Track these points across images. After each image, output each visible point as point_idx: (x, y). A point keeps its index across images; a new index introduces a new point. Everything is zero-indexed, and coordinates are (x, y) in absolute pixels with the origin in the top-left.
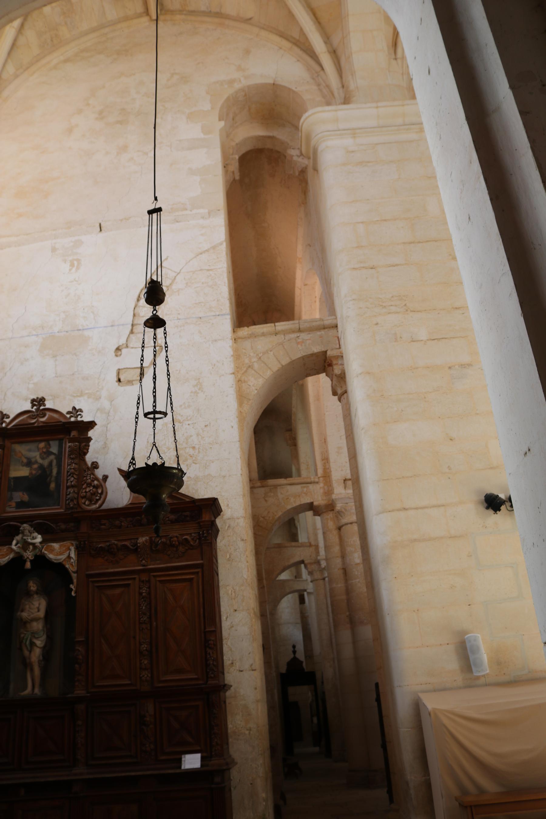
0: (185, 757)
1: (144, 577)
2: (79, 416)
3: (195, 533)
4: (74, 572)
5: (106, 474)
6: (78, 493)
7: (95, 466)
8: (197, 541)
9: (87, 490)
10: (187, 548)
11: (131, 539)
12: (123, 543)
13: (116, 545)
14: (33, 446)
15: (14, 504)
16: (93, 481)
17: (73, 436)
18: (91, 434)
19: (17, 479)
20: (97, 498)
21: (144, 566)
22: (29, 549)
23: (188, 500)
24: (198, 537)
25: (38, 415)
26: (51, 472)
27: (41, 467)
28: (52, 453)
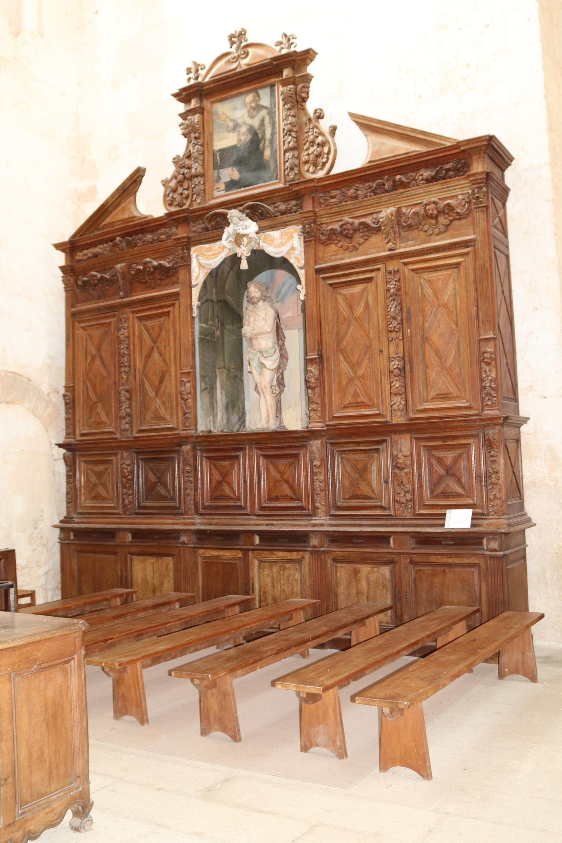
0: (450, 513)
1: (393, 266)
2: (293, 46)
3: (463, 194)
4: (301, 268)
5: (334, 124)
6: (298, 158)
9: (310, 152)
10: (451, 218)
11: (372, 214)
12: (361, 221)
13: (352, 224)
14: (237, 102)
15: (223, 186)
16: (317, 137)
17: (286, 76)
18: (311, 69)
20: (324, 160)
21: (390, 250)
22: (243, 243)
23: (448, 144)
24: (468, 200)
25: (239, 56)
26: (264, 134)
28: (263, 107)
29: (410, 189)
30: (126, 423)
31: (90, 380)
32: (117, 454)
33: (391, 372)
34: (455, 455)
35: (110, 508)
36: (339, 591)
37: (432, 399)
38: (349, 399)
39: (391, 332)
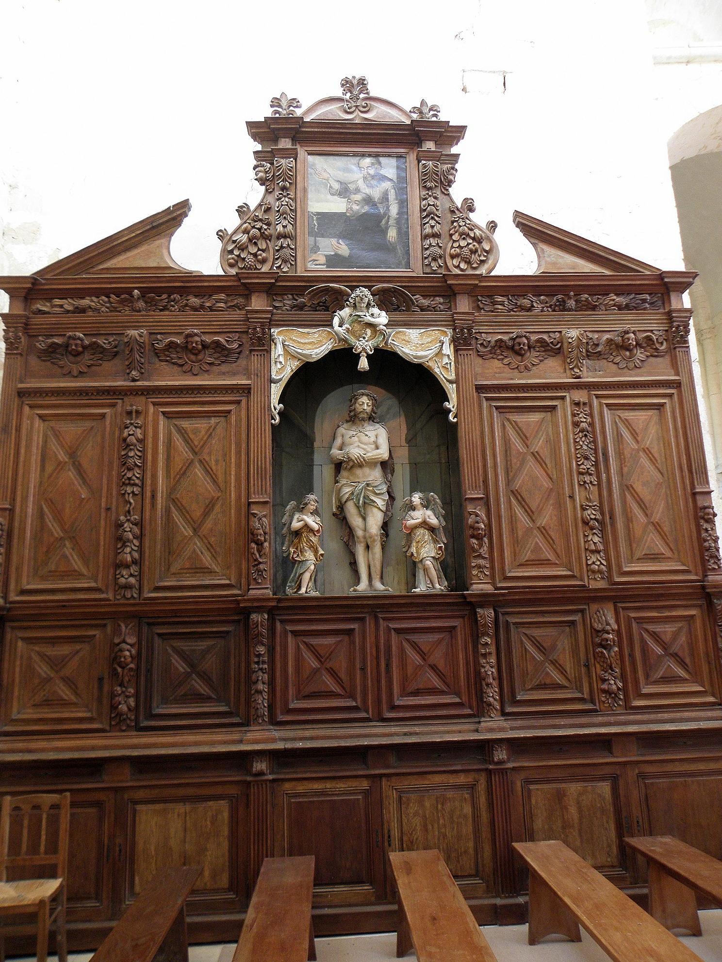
4: (451, 382)
7: (469, 205)
8: (665, 343)
15: (323, 260)
19: (325, 218)
27: (368, 200)
29: (601, 312)
30: (131, 575)
31: (51, 502)
32: (105, 625)
33: (586, 523)
34: (674, 629)
35: (81, 720)
36: (535, 828)
37: (639, 559)
38: (527, 555)
39: (582, 474)
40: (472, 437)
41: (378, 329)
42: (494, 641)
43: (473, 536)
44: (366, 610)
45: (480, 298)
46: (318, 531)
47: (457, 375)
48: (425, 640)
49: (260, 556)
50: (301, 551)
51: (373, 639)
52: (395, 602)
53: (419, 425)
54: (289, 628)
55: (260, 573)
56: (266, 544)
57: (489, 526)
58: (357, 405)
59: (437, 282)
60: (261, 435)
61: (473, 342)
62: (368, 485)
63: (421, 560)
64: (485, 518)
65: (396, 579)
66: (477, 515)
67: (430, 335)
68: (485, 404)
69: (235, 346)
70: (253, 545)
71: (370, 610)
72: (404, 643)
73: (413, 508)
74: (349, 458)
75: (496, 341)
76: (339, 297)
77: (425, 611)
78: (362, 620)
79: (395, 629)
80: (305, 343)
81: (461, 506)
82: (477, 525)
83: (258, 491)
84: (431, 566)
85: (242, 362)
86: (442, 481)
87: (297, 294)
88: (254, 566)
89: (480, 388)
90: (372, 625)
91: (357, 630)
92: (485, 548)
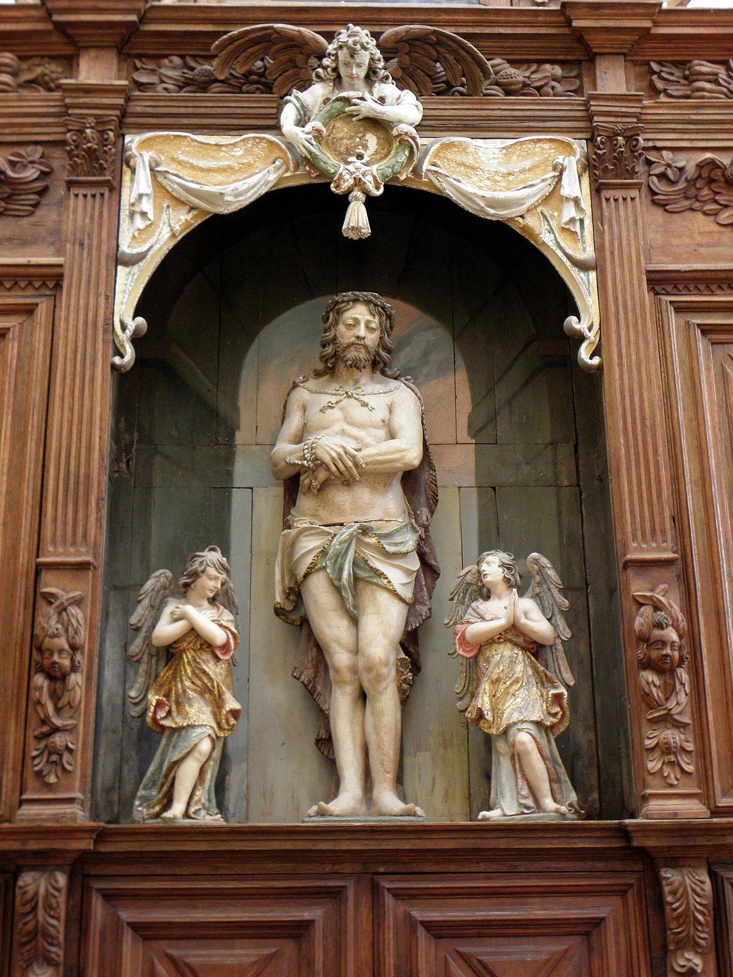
4: (582, 266)
40: (642, 401)
41: (395, 132)
42: (712, 965)
43: (647, 664)
44: (347, 868)
45: (655, 67)
46: (225, 647)
47: (599, 248)
48: (514, 958)
49: (58, 710)
50: (178, 703)
51: (366, 954)
52: (429, 845)
53: (502, 393)
54: (126, 915)
55: (54, 758)
56: (77, 679)
57: (691, 636)
58: (342, 328)
59: (548, 25)
60: (82, 391)
61: (640, 168)
62: (365, 531)
63: (505, 732)
64: (680, 616)
65: (440, 788)
66: (657, 607)
67: (528, 155)
68: (673, 321)
69: (31, 173)
70: (40, 680)
71: (358, 868)
72: (454, 966)
73: (485, 593)
74: (319, 463)
75: (700, 166)
76: (299, 58)
77: (513, 873)
78: (335, 895)
79: (429, 926)
80: (209, 170)
81: (613, 591)
82: (657, 633)
83: (64, 536)
84: (532, 746)
85: (47, 215)
86: (561, 534)
87: (194, 57)
88: (39, 738)
89: (660, 282)
90: (365, 912)
91: (319, 926)
92: (683, 698)
